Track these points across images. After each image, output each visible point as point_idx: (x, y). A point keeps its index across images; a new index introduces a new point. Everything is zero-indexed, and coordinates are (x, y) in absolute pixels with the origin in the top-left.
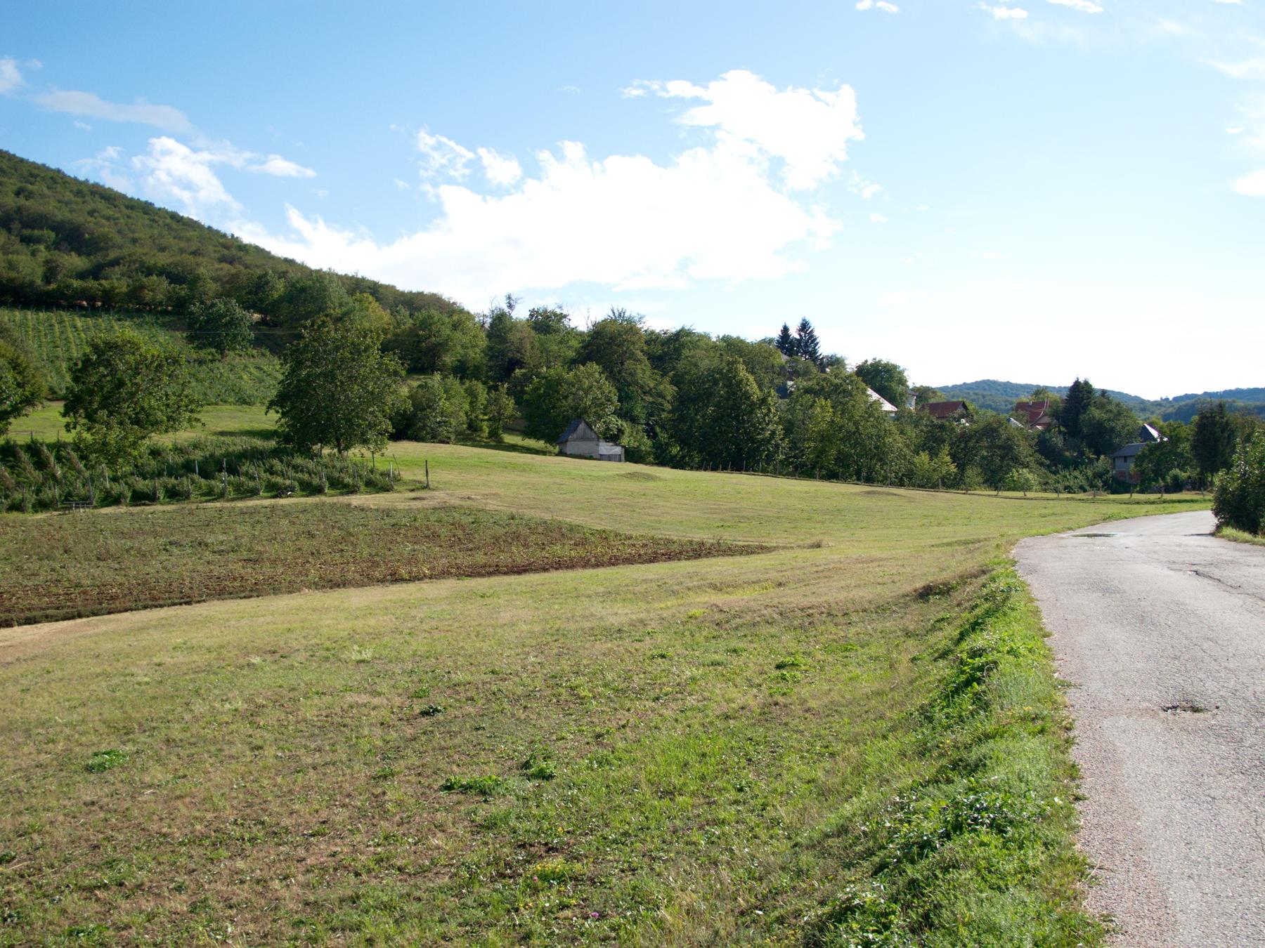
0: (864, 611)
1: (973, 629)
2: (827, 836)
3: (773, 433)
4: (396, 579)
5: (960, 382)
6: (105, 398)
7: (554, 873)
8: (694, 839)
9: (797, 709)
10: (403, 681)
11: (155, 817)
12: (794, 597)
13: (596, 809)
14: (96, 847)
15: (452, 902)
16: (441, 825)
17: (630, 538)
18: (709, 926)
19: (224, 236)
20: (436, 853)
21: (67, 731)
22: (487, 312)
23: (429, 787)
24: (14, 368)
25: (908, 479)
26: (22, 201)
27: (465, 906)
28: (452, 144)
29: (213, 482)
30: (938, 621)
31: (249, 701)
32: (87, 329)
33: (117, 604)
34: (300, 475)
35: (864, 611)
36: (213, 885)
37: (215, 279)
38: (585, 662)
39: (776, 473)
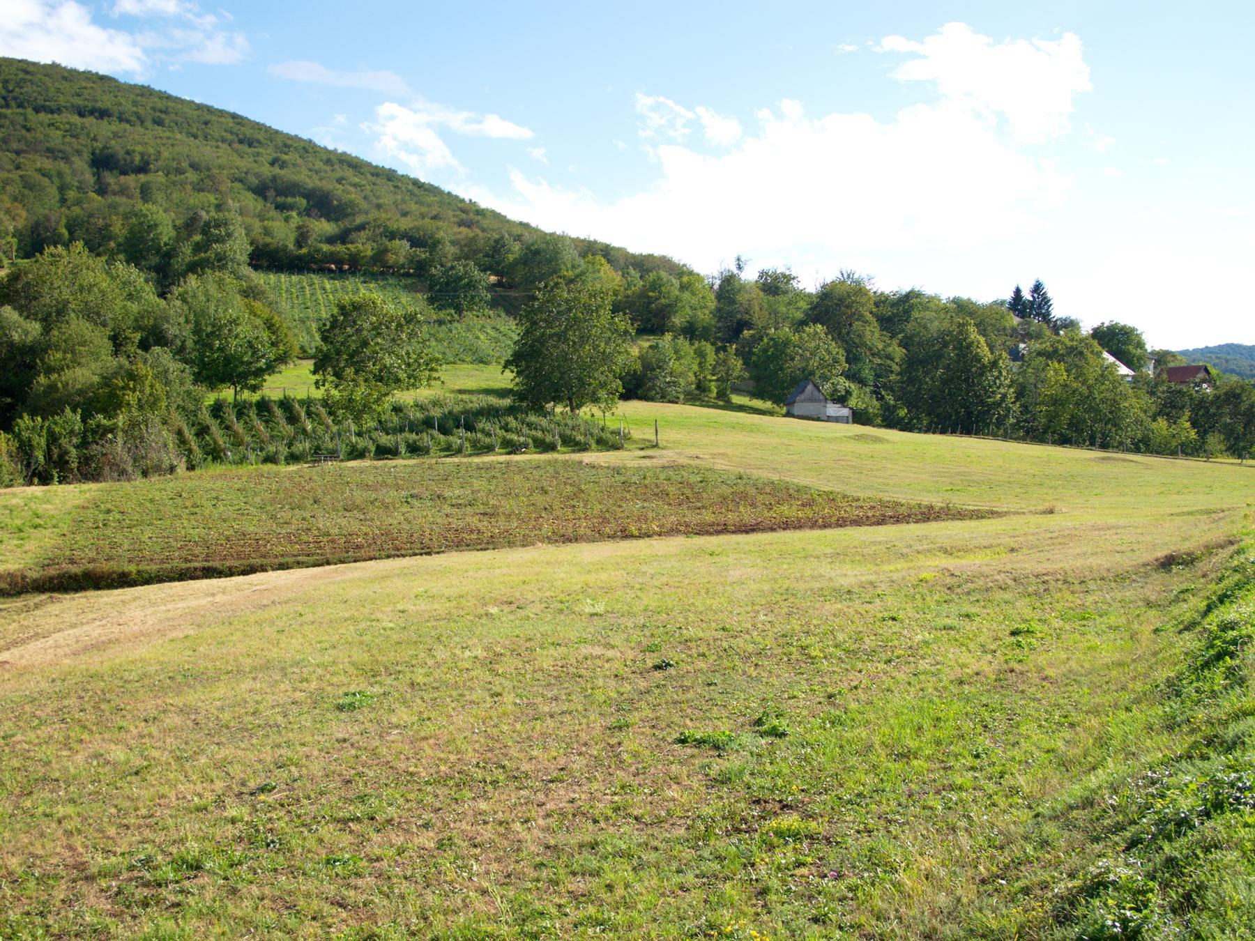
0: (1102, 579)
1: (1222, 602)
2: (1071, 808)
3: (1004, 396)
4: (626, 535)
5: (1201, 346)
6: (352, 356)
7: (789, 830)
8: (931, 803)
9: (1034, 677)
10: (636, 636)
11: (402, 757)
12: (1028, 564)
13: (831, 768)
14: (349, 782)
15: (688, 854)
16: (676, 778)
17: (858, 500)
18: (950, 892)
19: (463, 201)
20: (671, 805)
21: (320, 671)
22: (716, 274)
23: (663, 739)
24: (269, 328)
25: (1143, 445)
26: (276, 170)
27: (701, 858)
28: (670, 103)
29: (451, 438)
30: (1182, 592)
31: (487, 649)
32: (334, 291)
33: (362, 553)
34: (533, 432)
35: (1102, 579)
36: (458, 824)
37: (453, 243)
38: (815, 622)
39: (1006, 437)
